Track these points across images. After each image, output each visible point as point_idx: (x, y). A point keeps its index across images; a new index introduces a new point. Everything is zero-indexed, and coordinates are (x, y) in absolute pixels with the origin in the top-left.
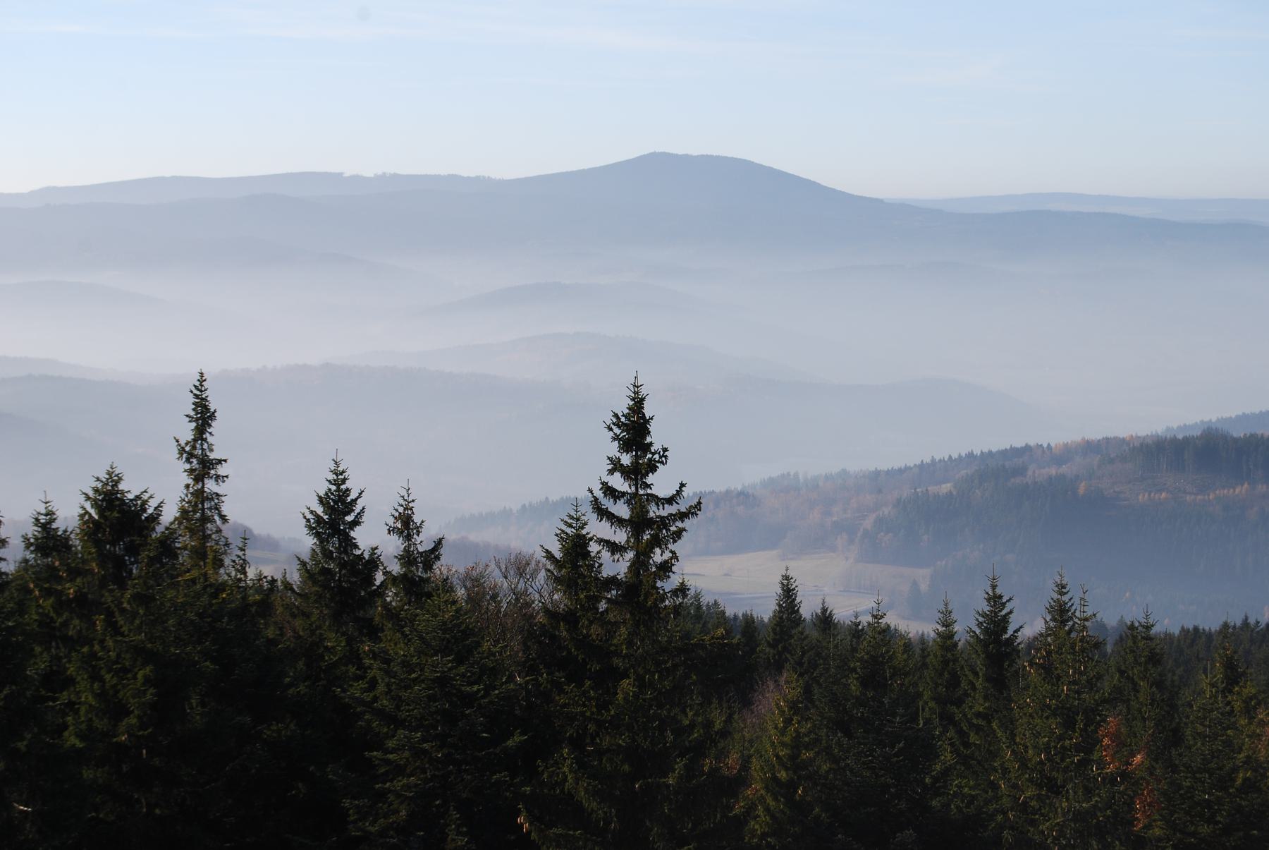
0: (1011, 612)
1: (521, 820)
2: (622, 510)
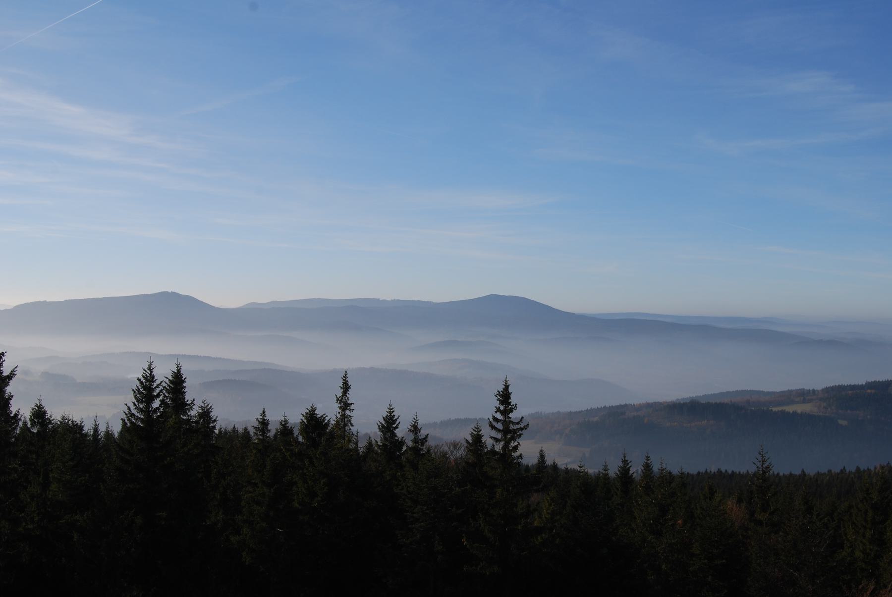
0: (631, 467)
1: (463, 540)
2: (500, 426)
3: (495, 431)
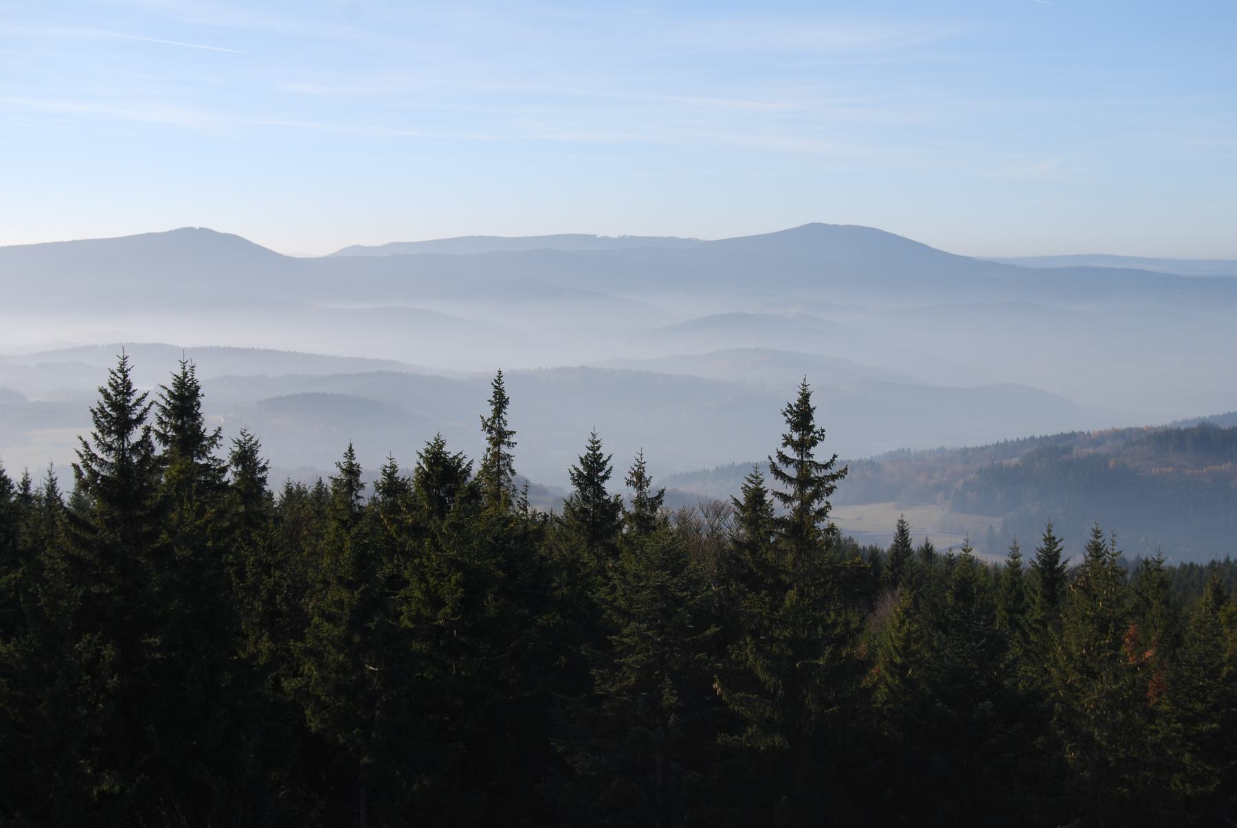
0: (1061, 549)
1: (715, 686)
2: (791, 472)
3: (782, 482)
